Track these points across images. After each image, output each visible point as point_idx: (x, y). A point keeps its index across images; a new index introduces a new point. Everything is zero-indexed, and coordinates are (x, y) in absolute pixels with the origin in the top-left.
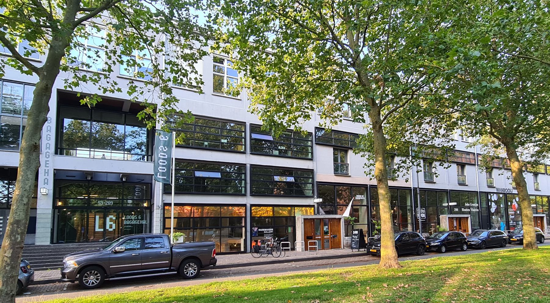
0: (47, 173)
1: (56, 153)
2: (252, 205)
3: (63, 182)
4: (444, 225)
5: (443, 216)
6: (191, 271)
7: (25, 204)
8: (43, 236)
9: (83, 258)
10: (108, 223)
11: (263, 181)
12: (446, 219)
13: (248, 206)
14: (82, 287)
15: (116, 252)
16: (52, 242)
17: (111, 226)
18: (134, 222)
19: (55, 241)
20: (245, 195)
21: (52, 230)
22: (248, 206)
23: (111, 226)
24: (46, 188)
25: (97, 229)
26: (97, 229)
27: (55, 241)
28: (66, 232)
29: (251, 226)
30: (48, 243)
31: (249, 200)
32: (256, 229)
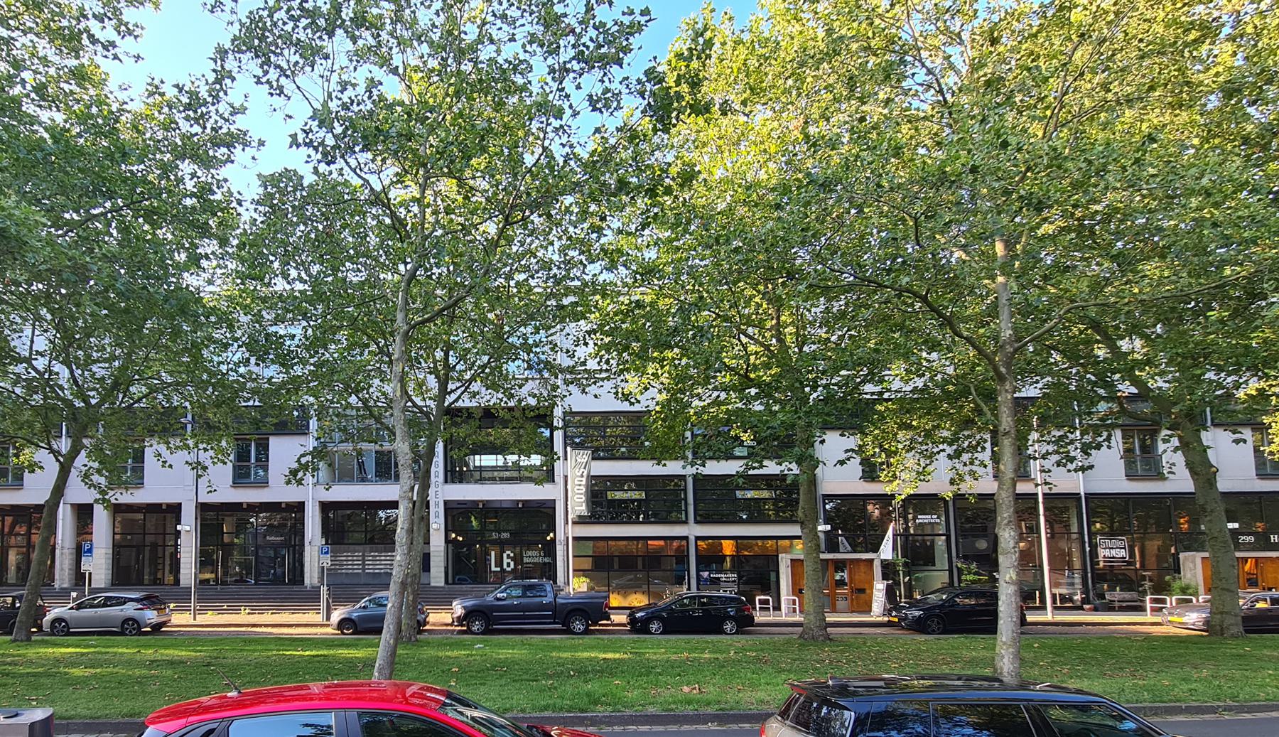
0: (437, 505)
1: (446, 482)
2: (698, 538)
3: (455, 511)
4: (1189, 575)
5: (1187, 554)
6: (578, 626)
7: (1246, 140)
8: (437, 576)
9: (469, 603)
10: (506, 561)
11: (717, 500)
12: (1194, 562)
13: (692, 539)
14: (647, 631)
15: (499, 599)
16: (447, 582)
17: (509, 565)
18: (535, 560)
19: (450, 580)
20: (686, 522)
21: (446, 568)
22: (692, 539)
23: (509, 565)
24: (437, 523)
25: (493, 569)
26: (493, 569)
27: (450, 580)
28: (466, 567)
29: (698, 571)
30: (442, 584)
31: (693, 530)
32: (705, 574)
